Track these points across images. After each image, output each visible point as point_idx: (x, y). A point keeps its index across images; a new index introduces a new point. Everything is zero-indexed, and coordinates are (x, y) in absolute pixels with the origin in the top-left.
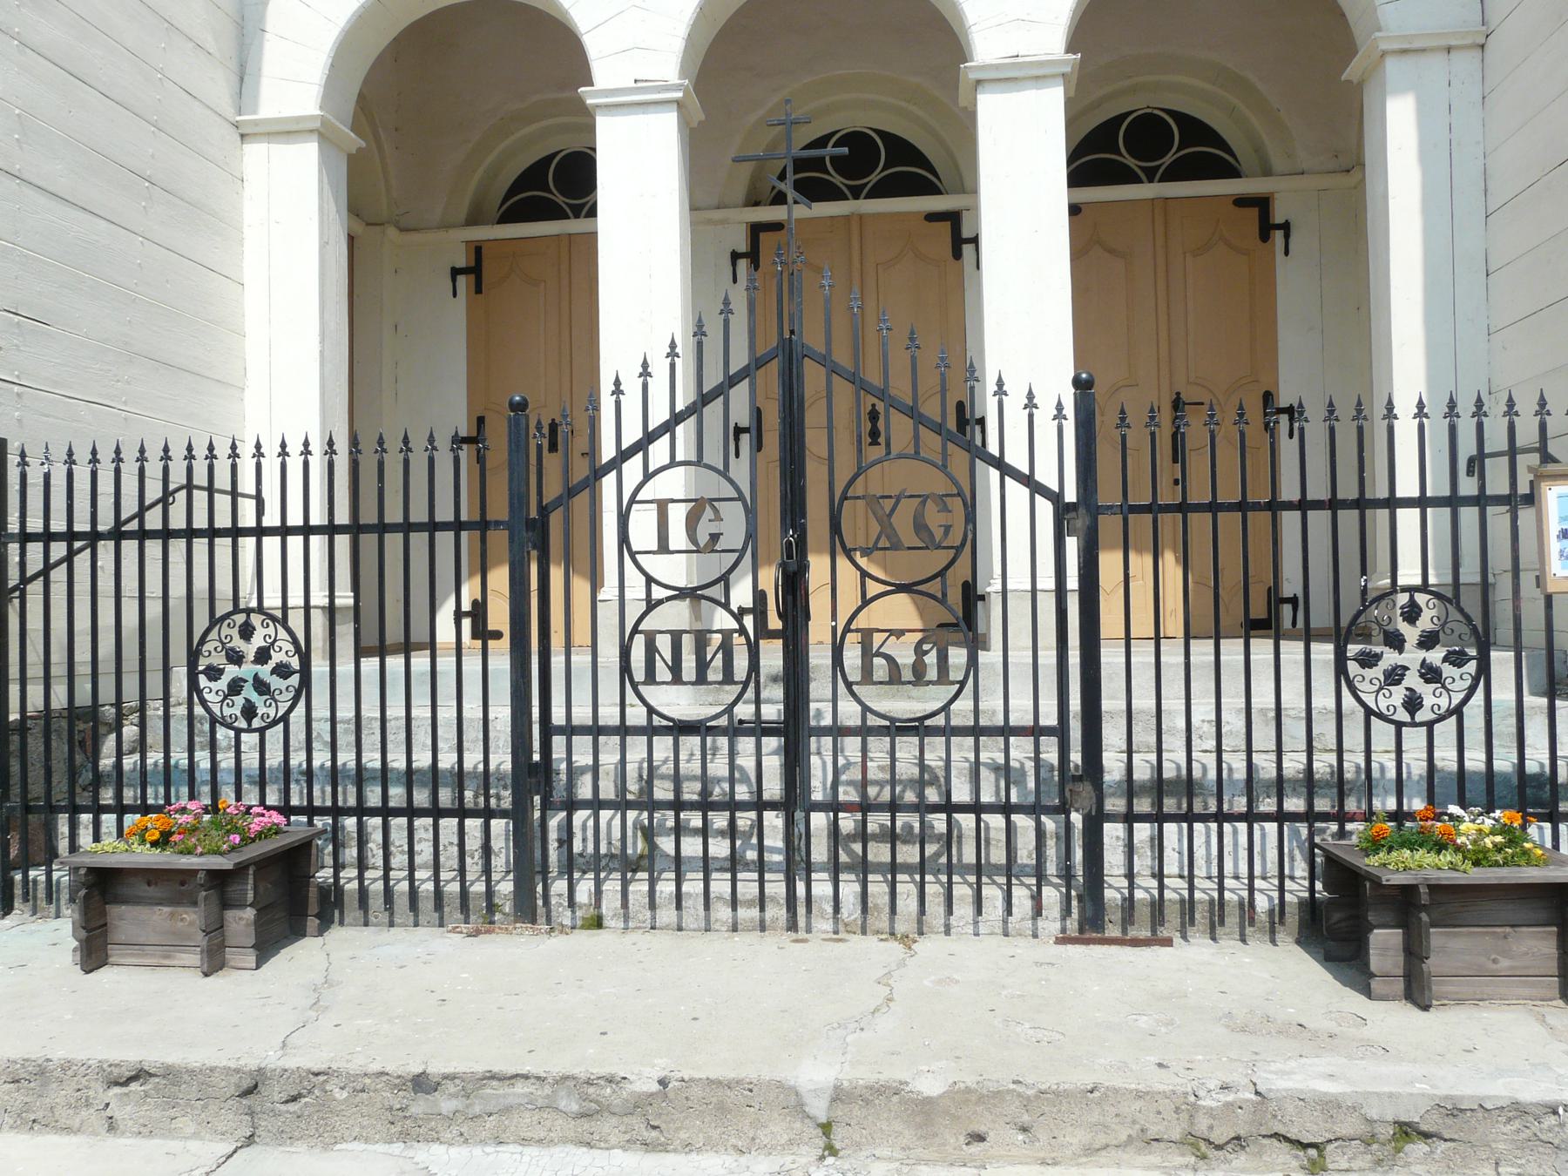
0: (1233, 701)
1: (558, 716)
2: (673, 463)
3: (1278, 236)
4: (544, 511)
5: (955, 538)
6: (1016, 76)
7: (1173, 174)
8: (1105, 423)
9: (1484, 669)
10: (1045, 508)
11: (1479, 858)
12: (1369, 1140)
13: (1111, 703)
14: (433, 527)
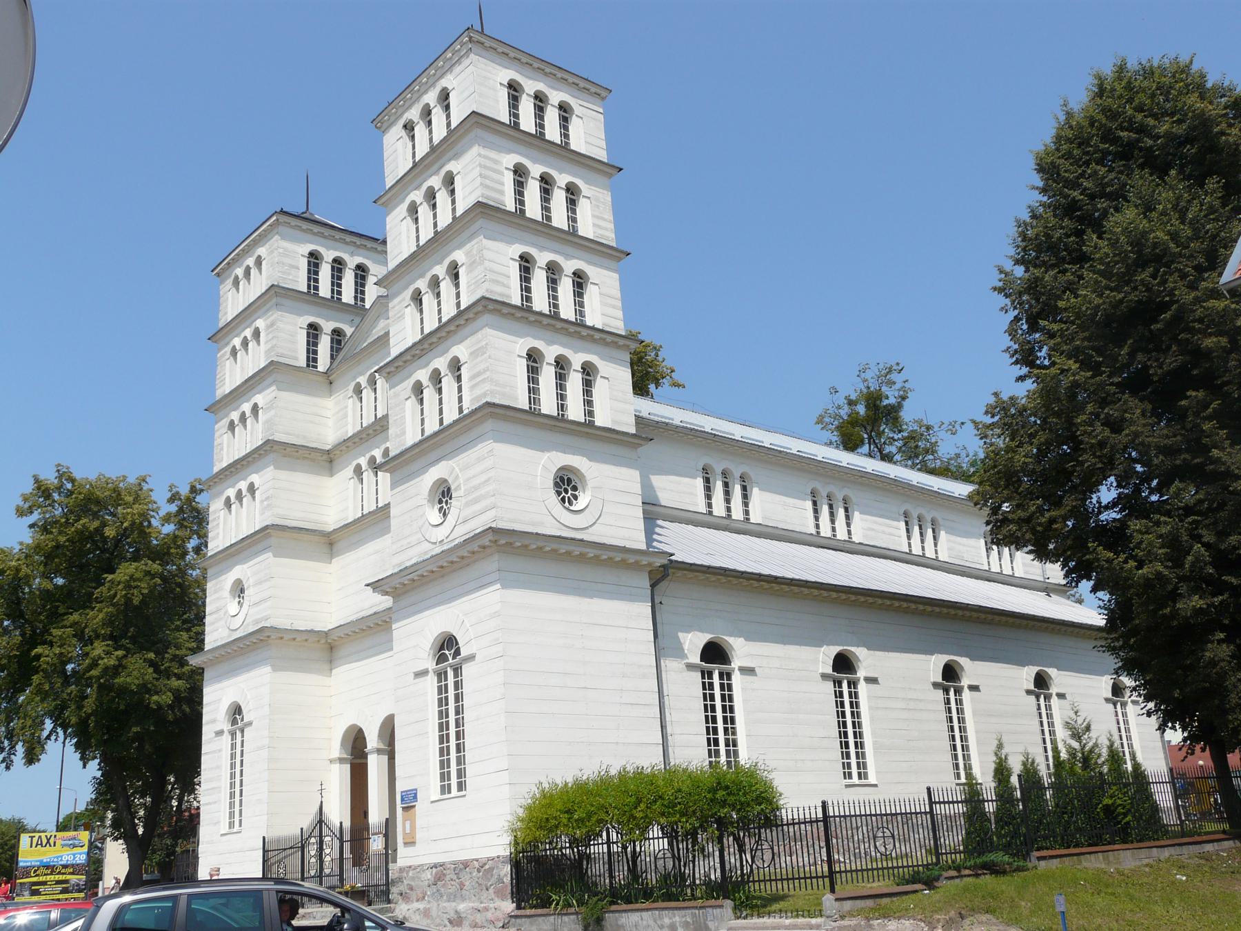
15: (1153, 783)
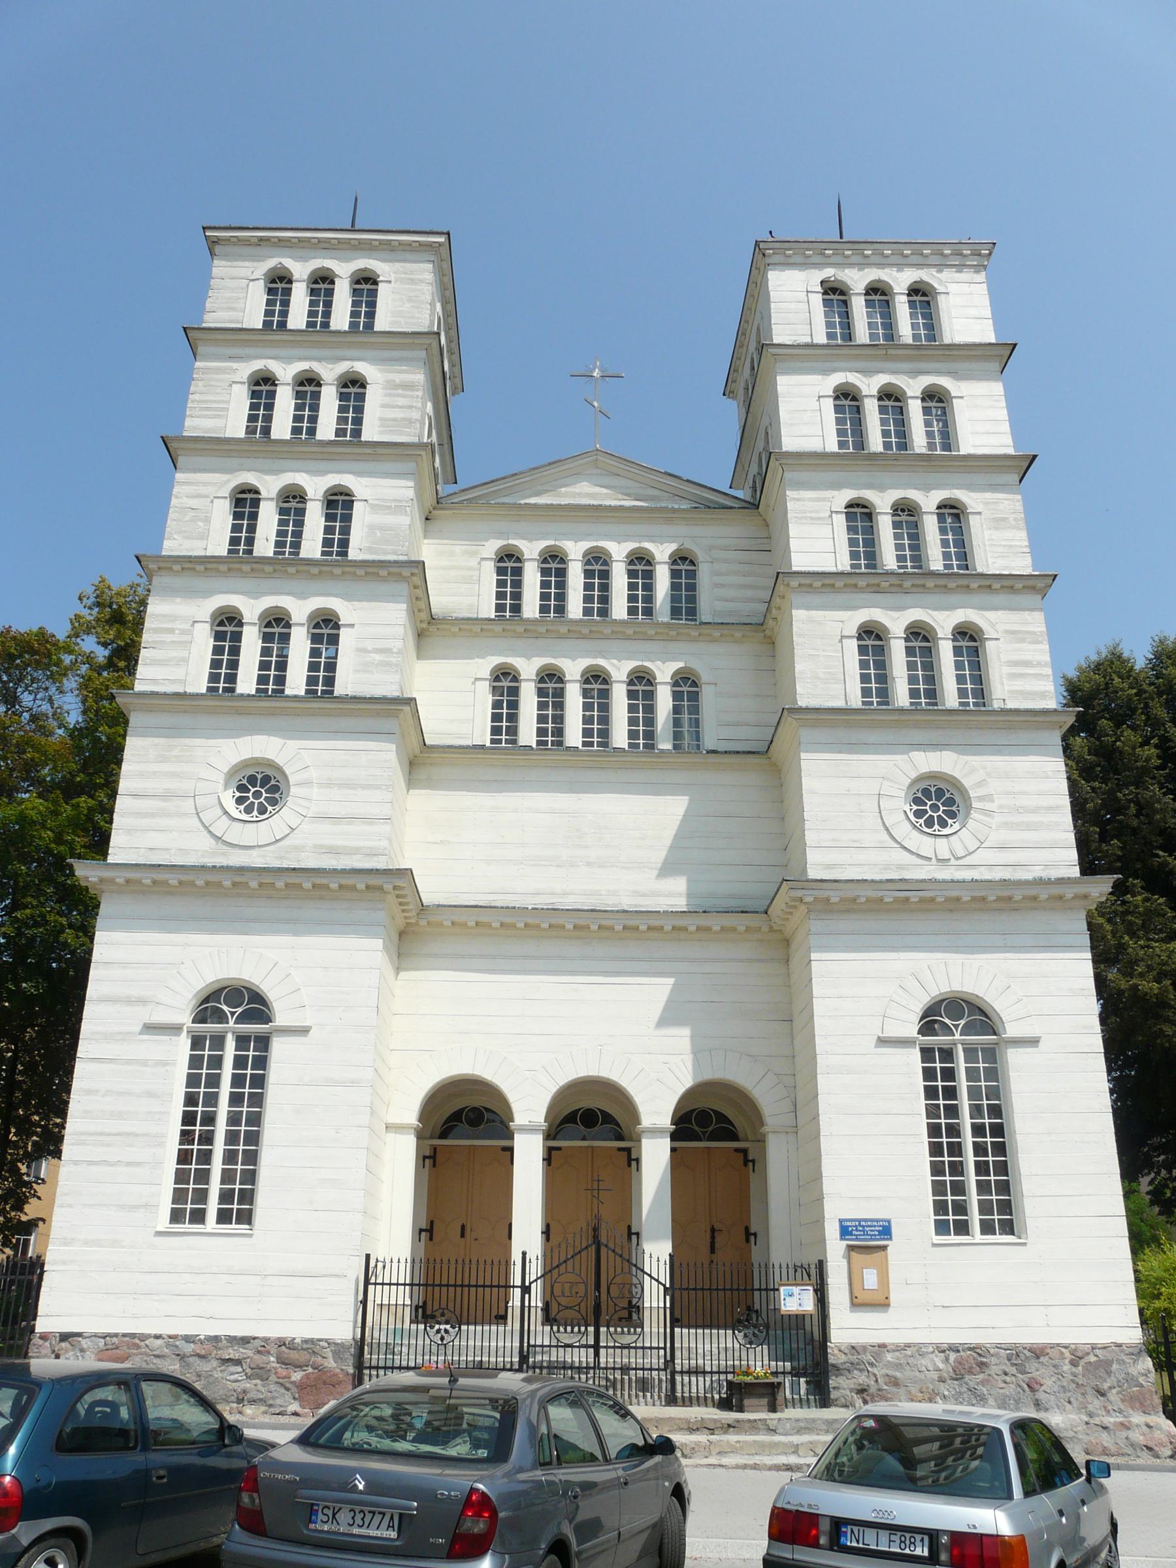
0: (715, 1345)
1: (532, 1342)
2: (566, 1272)
3: (751, 1164)
4: (530, 1283)
5: (638, 1296)
6: (655, 1132)
7: (712, 1138)
8: (677, 1265)
9: (767, 1333)
10: (661, 1288)
11: (757, 1378)
12: (722, 1428)
13: (677, 1345)
14: (760, 1290)
15: (405, 1285)
